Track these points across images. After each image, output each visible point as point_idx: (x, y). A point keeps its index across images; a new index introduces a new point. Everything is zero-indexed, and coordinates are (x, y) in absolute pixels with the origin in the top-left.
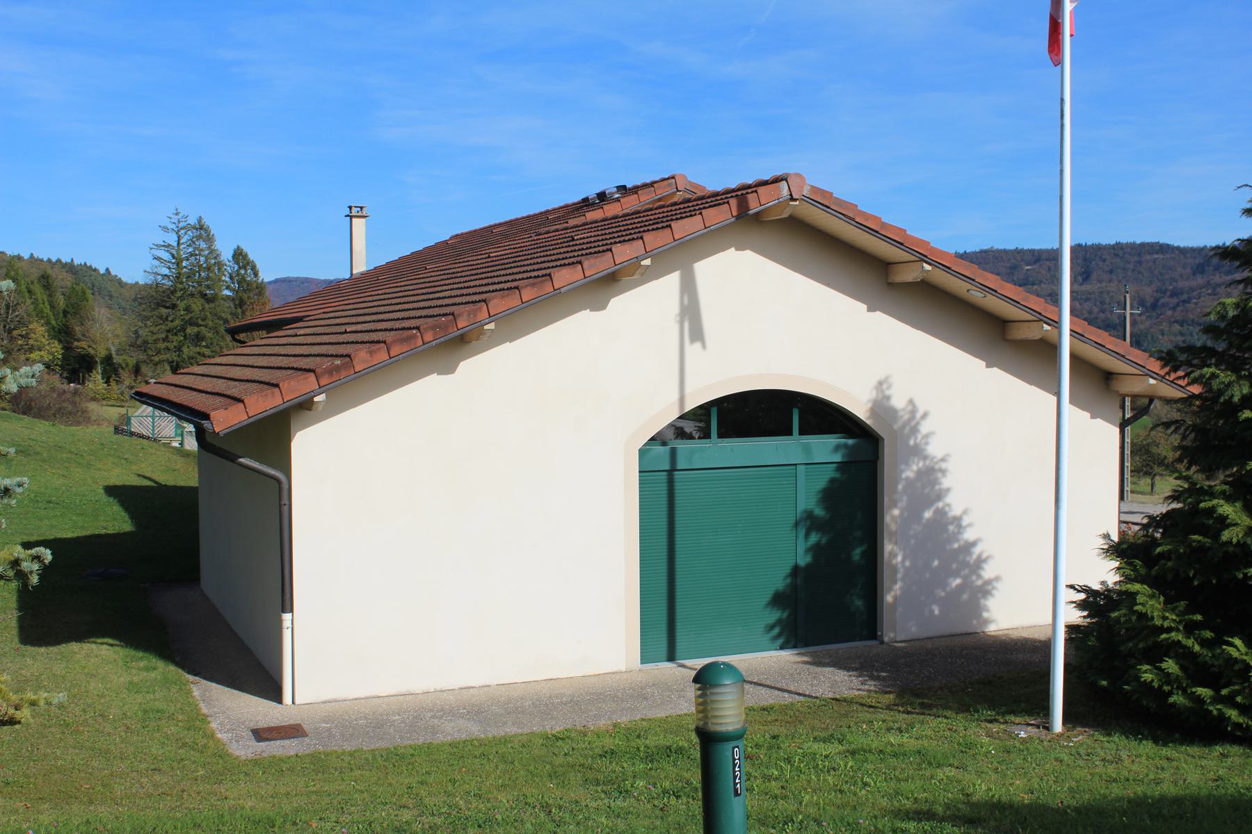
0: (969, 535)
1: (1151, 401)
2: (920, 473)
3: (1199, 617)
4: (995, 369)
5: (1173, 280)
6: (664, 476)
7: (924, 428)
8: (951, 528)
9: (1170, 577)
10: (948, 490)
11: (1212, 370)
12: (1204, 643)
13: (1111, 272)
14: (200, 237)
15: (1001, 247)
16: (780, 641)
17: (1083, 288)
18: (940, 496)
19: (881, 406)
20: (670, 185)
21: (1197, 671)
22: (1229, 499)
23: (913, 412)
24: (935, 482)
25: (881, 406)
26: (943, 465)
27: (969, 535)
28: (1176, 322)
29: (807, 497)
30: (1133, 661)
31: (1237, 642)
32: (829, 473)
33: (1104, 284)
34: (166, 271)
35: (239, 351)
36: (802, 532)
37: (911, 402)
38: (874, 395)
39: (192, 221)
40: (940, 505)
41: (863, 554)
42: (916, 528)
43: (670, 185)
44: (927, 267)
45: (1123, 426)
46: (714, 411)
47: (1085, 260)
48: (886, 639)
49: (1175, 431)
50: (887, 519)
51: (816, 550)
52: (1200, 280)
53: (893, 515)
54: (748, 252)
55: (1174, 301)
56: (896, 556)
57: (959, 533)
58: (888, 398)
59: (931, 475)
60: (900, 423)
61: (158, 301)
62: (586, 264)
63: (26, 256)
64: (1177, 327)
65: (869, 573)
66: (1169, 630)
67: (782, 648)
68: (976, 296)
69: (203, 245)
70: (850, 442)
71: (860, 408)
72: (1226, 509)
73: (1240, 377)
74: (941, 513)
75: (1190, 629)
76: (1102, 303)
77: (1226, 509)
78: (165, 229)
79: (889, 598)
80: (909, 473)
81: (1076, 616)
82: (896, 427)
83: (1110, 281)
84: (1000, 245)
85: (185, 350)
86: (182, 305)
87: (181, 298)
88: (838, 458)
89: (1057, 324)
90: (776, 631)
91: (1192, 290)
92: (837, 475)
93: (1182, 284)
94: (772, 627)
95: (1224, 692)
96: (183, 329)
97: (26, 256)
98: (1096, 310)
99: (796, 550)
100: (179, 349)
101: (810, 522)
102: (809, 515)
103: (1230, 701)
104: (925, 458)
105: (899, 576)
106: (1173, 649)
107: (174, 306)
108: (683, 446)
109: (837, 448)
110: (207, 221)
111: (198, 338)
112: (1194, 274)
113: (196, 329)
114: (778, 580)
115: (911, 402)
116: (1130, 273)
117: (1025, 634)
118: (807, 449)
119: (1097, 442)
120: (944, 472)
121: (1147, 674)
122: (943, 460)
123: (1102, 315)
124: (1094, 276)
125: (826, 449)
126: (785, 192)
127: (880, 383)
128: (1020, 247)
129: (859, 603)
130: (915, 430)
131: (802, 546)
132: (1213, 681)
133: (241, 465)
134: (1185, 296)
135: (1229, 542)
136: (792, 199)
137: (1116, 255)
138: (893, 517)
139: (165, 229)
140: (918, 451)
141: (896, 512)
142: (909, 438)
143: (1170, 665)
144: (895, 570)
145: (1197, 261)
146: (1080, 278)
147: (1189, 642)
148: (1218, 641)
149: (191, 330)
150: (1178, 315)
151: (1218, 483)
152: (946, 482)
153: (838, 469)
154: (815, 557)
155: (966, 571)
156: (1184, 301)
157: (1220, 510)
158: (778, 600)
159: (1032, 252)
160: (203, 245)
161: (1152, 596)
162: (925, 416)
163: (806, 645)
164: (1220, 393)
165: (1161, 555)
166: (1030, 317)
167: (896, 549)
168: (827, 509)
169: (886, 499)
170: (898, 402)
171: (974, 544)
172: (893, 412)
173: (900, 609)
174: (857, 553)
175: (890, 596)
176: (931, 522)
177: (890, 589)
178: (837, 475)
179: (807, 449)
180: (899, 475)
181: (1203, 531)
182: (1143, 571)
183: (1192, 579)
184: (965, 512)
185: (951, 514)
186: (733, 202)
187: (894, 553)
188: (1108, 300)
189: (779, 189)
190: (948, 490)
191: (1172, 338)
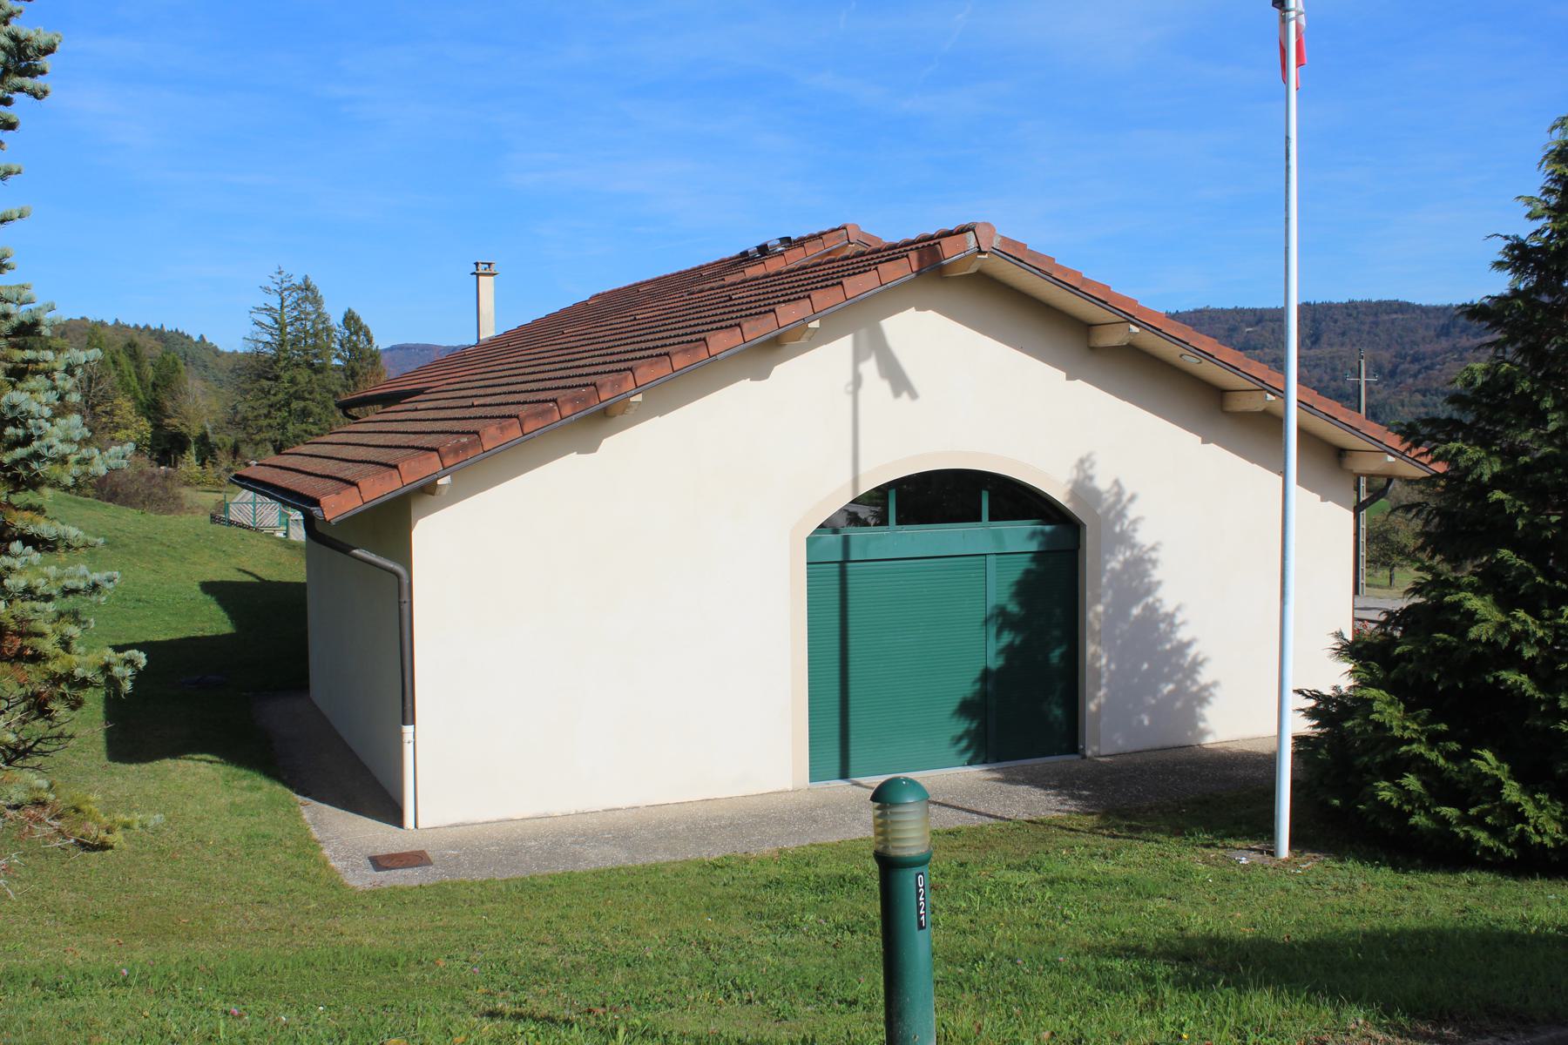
0: (1183, 635)
1: (1390, 481)
2: (1126, 563)
3: (1444, 727)
5: (1414, 343)
6: (835, 568)
7: (1132, 513)
8: (1162, 626)
9: (1411, 682)
10: (1159, 583)
11: (1458, 445)
12: (1449, 756)
13: (1343, 334)
14: (305, 299)
15: (1218, 306)
16: (969, 755)
17: (1312, 352)
19: (1082, 488)
20: (840, 237)
21: (1442, 788)
22: (1478, 591)
23: (1119, 494)
25: (1082, 488)
26: (1154, 555)
27: (1183, 635)
29: (999, 590)
30: (1368, 777)
31: (1488, 754)
32: (1024, 563)
34: (268, 338)
36: (993, 630)
37: (1117, 482)
38: (1074, 475)
39: (298, 281)
40: (1150, 600)
41: (1062, 656)
44: (1134, 329)
45: (1358, 509)
48: (1089, 753)
50: (1090, 616)
51: (1009, 652)
52: (1444, 343)
53: (1096, 612)
55: (1416, 367)
56: (1099, 658)
57: (1172, 632)
58: (1091, 478)
59: (1139, 566)
60: (1105, 505)
61: (259, 371)
63: (110, 322)
64: (1419, 397)
65: (1068, 680)
66: (1410, 741)
67: (970, 763)
68: (1191, 362)
69: (310, 308)
70: (1048, 528)
71: (1057, 488)
72: (1474, 603)
74: (1151, 610)
75: (1434, 740)
76: (1334, 370)
77: (1474, 603)
78: (267, 290)
79: (1092, 707)
80: (1115, 564)
81: (1303, 726)
82: (1099, 511)
85: (290, 427)
86: (286, 376)
87: (285, 369)
88: (1033, 546)
89: (1282, 393)
90: (964, 743)
91: (1435, 354)
92: (1033, 566)
94: (959, 739)
95: (1472, 811)
96: (288, 404)
97: (110, 322)
98: (1326, 378)
99: (989, 651)
100: (283, 426)
101: (1002, 619)
102: (1001, 612)
103: (1478, 821)
104: (1133, 546)
105: (1104, 681)
106: (1416, 764)
107: (277, 378)
108: (856, 534)
109: (1033, 535)
110: (313, 281)
111: (305, 414)
113: (302, 404)
114: (966, 686)
115: (1117, 482)
116: (1365, 336)
117: (1247, 748)
118: (998, 537)
122: (1153, 549)
123: (1333, 384)
124: (1324, 339)
125: (1020, 536)
126: (972, 244)
127: (1082, 461)
129: (1058, 712)
130: (1121, 515)
131: (994, 646)
134: (1428, 362)
135: (1478, 641)
136: (980, 252)
137: (1350, 315)
138: (1097, 615)
139: (267, 290)
140: (1124, 539)
141: (1100, 608)
142: (1114, 524)
143: (1412, 782)
144: (1098, 673)
147: (1433, 755)
148: (1465, 755)
149: (296, 405)
152: (1156, 575)
153: (1033, 560)
154: (1009, 660)
155: (1180, 676)
156: (1427, 368)
158: (966, 708)
159: (1254, 311)
160: (310, 308)
162: (1132, 498)
164: (1468, 470)
165: (1401, 656)
167: (1100, 650)
168: (1021, 604)
169: (1088, 594)
170: (1102, 483)
171: (1189, 644)
172: (1096, 495)
174: (1055, 655)
175: (1095, 702)
177: (1093, 696)
178: (1033, 566)
179: (998, 537)
183: (1436, 684)
184: (1178, 608)
185: (1162, 611)
186: (913, 255)
187: (1097, 655)
189: (966, 242)
190: (1159, 583)
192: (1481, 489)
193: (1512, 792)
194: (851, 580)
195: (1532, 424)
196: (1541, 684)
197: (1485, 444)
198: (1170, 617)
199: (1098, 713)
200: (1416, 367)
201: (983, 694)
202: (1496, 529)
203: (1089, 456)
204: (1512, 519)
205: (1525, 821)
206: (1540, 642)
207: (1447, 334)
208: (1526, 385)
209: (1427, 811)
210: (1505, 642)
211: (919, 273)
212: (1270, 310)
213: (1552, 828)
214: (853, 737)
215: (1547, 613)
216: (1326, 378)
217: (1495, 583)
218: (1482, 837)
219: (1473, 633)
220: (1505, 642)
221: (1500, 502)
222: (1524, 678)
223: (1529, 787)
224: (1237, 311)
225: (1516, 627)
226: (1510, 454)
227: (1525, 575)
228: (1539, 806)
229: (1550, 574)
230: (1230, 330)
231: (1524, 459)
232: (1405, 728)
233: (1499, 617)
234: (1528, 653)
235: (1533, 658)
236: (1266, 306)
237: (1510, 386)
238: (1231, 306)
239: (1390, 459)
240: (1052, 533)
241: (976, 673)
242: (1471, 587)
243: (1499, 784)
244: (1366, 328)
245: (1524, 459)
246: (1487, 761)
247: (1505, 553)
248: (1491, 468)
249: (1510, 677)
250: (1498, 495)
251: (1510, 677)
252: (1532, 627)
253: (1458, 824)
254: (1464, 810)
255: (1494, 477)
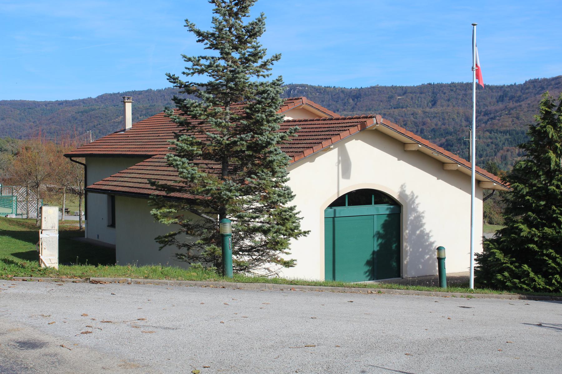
0: (432, 240)
1: (494, 191)
2: (415, 218)
3: (514, 259)
4: (440, 180)
6: (331, 219)
7: (417, 201)
8: (426, 237)
9: (505, 248)
10: (424, 224)
11: (517, 184)
12: (515, 267)
13: (449, 100)
15: (383, 85)
16: (369, 277)
17: (432, 110)
18: (422, 226)
19: (402, 194)
20: (300, 102)
21: (514, 275)
22: (523, 224)
23: (413, 196)
24: (421, 221)
25: (402, 194)
26: (423, 215)
27: (432, 240)
28: (487, 131)
29: (377, 227)
30: (494, 274)
31: (526, 266)
32: (385, 218)
33: (444, 108)
35: (153, 177)
36: (376, 239)
37: (412, 192)
38: (400, 190)
40: (422, 229)
41: (396, 247)
42: (414, 237)
43: (300, 102)
44: (420, 146)
45: (484, 200)
46: (347, 197)
47: (433, 93)
48: (404, 277)
49: (506, 203)
50: (404, 234)
51: (381, 245)
52: (501, 105)
53: (406, 232)
54: (359, 141)
55: (486, 118)
56: (407, 247)
57: (428, 239)
58: (405, 191)
59: (419, 218)
60: (409, 200)
62: (314, 148)
64: (488, 134)
65: (398, 254)
66: (506, 263)
67: (369, 280)
68: (435, 155)
70: (392, 207)
71: (395, 194)
73: (526, 186)
74: (422, 232)
75: (512, 263)
76: (443, 119)
79: (405, 262)
80: (412, 218)
81: (475, 264)
82: (407, 201)
83: (448, 106)
84: (382, 84)
88: (388, 212)
89: (471, 169)
90: (368, 274)
91: (496, 111)
92: (387, 219)
93: (491, 108)
94: (366, 272)
95: (522, 280)
98: (440, 123)
101: (379, 235)
102: (378, 233)
103: (524, 283)
104: (417, 212)
105: (408, 254)
108: (338, 209)
109: (388, 209)
112: (498, 102)
115: (412, 192)
116: (460, 101)
117: (451, 275)
118: (377, 210)
119: (479, 204)
120: (423, 217)
121: (499, 277)
122: (423, 213)
123: (443, 127)
124: (439, 103)
125: (384, 209)
126: (375, 122)
127: (402, 186)
128: (394, 85)
129: (394, 264)
130: (413, 202)
131: (376, 244)
132: (519, 278)
133: (202, 216)
134: (492, 115)
135: (523, 236)
136: (377, 124)
137: (452, 90)
138: (406, 234)
140: (415, 210)
141: (407, 231)
142: (411, 205)
143: (506, 274)
144: (407, 252)
145: (499, 94)
146: (430, 104)
147: (512, 266)
150: (488, 127)
151: (519, 218)
152: (424, 221)
153: (387, 216)
154: (380, 248)
155: (431, 253)
156: (492, 118)
157: (520, 227)
158: (368, 263)
159: (402, 88)
161: (501, 253)
162: (417, 197)
163: (377, 279)
164: (520, 191)
165: (502, 241)
166: (453, 162)
167: (407, 245)
168: (384, 231)
169: (404, 227)
170: (408, 192)
171: (433, 243)
172: (406, 196)
173: (409, 266)
175: (406, 261)
176: (419, 235)
177: (406, 259)
178: (387, 219)
179: (377, 210)
180: (408, 219)
181: (516, 233)
182: (497, 246)
183: (512, 248)
184: (430, 231)
185: (426, 232)
186: (359, 126)
187: (407, 246)
188: (447, 118)
189: (373, 121)
190: (424, 224)
191: (485, 140)
192: (523, 196)
193: (532, 275)
194: (336, 223)
195: (537, 179)
196: (539, 248)
197: (525, 184)
198: (428, 234)
199: (407, 265)
200: (486, 118)
201: (373, 258)
202: (528, 207)
203: (404, 184)
204: (532, 204)
205: (535, 281)
206: (539, 236)
207: (502, 101)
208: (535, 169)
209: (511, 282)
210: (530, 236)
211: (360, 131)
212: (410, 87)
213: (542, 283)
214: (336, 271)
215: (540, 229)
216: (440, 123)
217: (526, 221)
218: (525, 286)
219: (522, 234)
220: (530, 236)
221: (529, 199)
222: (535, 246)
223: (536, 273)
224: (393, 88)
225: (533, 232)
226: (531, 186)
227: (535, 219)
228: (539, 278)
229: (541, 219)
230: (389, 97)
231: (535, 188)
232: (504, 260)
233: (528, 230)
234: (536, 239)
235: (537, 241)
236: (408, 85)
237: (531, 168)
238: (390, 85)
239: (495, 184)
240: (393, 208)
241: (371, 252)
242: (521, 222)
243: (529, 273)
244: (460, 97)
245: (535, 188)
246: (526, 267)
247: (530, 213)
248: (526, 190)
249: (531, 246)
250: (528, 197)
251: (531, 246)
252: (537, 233)
253: (537, 148)
254: (520, 280)
255: (527, 193)
